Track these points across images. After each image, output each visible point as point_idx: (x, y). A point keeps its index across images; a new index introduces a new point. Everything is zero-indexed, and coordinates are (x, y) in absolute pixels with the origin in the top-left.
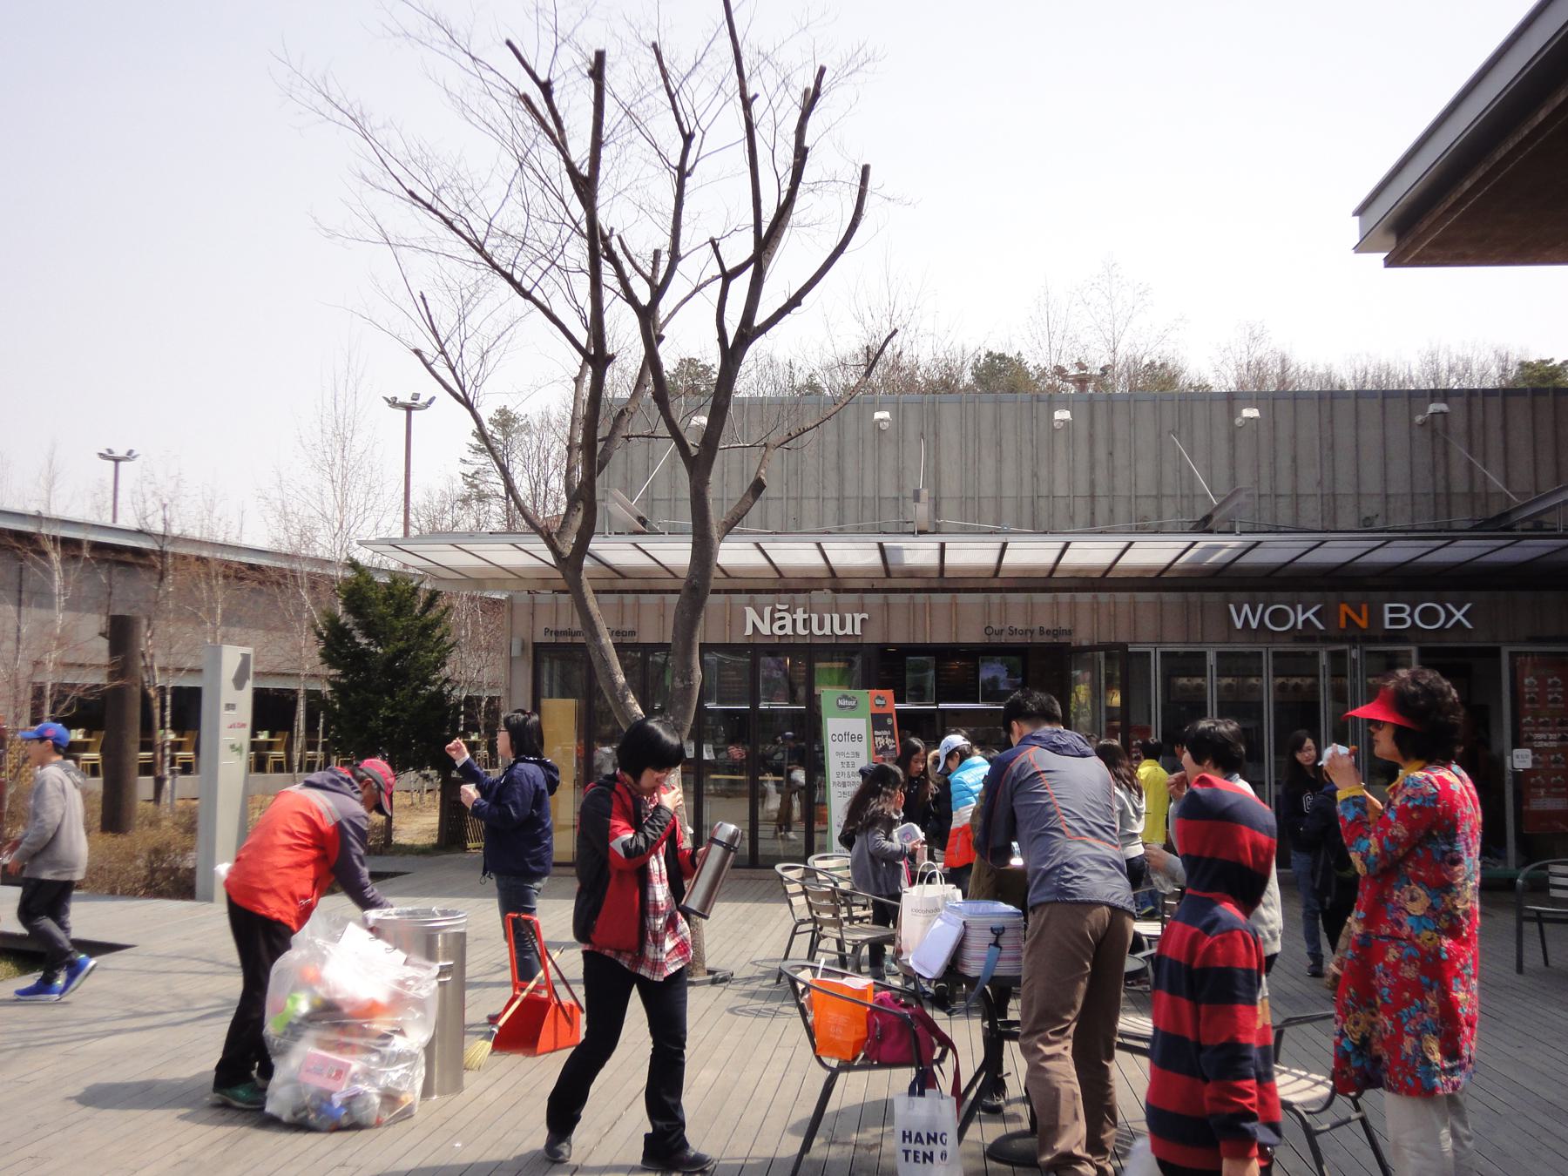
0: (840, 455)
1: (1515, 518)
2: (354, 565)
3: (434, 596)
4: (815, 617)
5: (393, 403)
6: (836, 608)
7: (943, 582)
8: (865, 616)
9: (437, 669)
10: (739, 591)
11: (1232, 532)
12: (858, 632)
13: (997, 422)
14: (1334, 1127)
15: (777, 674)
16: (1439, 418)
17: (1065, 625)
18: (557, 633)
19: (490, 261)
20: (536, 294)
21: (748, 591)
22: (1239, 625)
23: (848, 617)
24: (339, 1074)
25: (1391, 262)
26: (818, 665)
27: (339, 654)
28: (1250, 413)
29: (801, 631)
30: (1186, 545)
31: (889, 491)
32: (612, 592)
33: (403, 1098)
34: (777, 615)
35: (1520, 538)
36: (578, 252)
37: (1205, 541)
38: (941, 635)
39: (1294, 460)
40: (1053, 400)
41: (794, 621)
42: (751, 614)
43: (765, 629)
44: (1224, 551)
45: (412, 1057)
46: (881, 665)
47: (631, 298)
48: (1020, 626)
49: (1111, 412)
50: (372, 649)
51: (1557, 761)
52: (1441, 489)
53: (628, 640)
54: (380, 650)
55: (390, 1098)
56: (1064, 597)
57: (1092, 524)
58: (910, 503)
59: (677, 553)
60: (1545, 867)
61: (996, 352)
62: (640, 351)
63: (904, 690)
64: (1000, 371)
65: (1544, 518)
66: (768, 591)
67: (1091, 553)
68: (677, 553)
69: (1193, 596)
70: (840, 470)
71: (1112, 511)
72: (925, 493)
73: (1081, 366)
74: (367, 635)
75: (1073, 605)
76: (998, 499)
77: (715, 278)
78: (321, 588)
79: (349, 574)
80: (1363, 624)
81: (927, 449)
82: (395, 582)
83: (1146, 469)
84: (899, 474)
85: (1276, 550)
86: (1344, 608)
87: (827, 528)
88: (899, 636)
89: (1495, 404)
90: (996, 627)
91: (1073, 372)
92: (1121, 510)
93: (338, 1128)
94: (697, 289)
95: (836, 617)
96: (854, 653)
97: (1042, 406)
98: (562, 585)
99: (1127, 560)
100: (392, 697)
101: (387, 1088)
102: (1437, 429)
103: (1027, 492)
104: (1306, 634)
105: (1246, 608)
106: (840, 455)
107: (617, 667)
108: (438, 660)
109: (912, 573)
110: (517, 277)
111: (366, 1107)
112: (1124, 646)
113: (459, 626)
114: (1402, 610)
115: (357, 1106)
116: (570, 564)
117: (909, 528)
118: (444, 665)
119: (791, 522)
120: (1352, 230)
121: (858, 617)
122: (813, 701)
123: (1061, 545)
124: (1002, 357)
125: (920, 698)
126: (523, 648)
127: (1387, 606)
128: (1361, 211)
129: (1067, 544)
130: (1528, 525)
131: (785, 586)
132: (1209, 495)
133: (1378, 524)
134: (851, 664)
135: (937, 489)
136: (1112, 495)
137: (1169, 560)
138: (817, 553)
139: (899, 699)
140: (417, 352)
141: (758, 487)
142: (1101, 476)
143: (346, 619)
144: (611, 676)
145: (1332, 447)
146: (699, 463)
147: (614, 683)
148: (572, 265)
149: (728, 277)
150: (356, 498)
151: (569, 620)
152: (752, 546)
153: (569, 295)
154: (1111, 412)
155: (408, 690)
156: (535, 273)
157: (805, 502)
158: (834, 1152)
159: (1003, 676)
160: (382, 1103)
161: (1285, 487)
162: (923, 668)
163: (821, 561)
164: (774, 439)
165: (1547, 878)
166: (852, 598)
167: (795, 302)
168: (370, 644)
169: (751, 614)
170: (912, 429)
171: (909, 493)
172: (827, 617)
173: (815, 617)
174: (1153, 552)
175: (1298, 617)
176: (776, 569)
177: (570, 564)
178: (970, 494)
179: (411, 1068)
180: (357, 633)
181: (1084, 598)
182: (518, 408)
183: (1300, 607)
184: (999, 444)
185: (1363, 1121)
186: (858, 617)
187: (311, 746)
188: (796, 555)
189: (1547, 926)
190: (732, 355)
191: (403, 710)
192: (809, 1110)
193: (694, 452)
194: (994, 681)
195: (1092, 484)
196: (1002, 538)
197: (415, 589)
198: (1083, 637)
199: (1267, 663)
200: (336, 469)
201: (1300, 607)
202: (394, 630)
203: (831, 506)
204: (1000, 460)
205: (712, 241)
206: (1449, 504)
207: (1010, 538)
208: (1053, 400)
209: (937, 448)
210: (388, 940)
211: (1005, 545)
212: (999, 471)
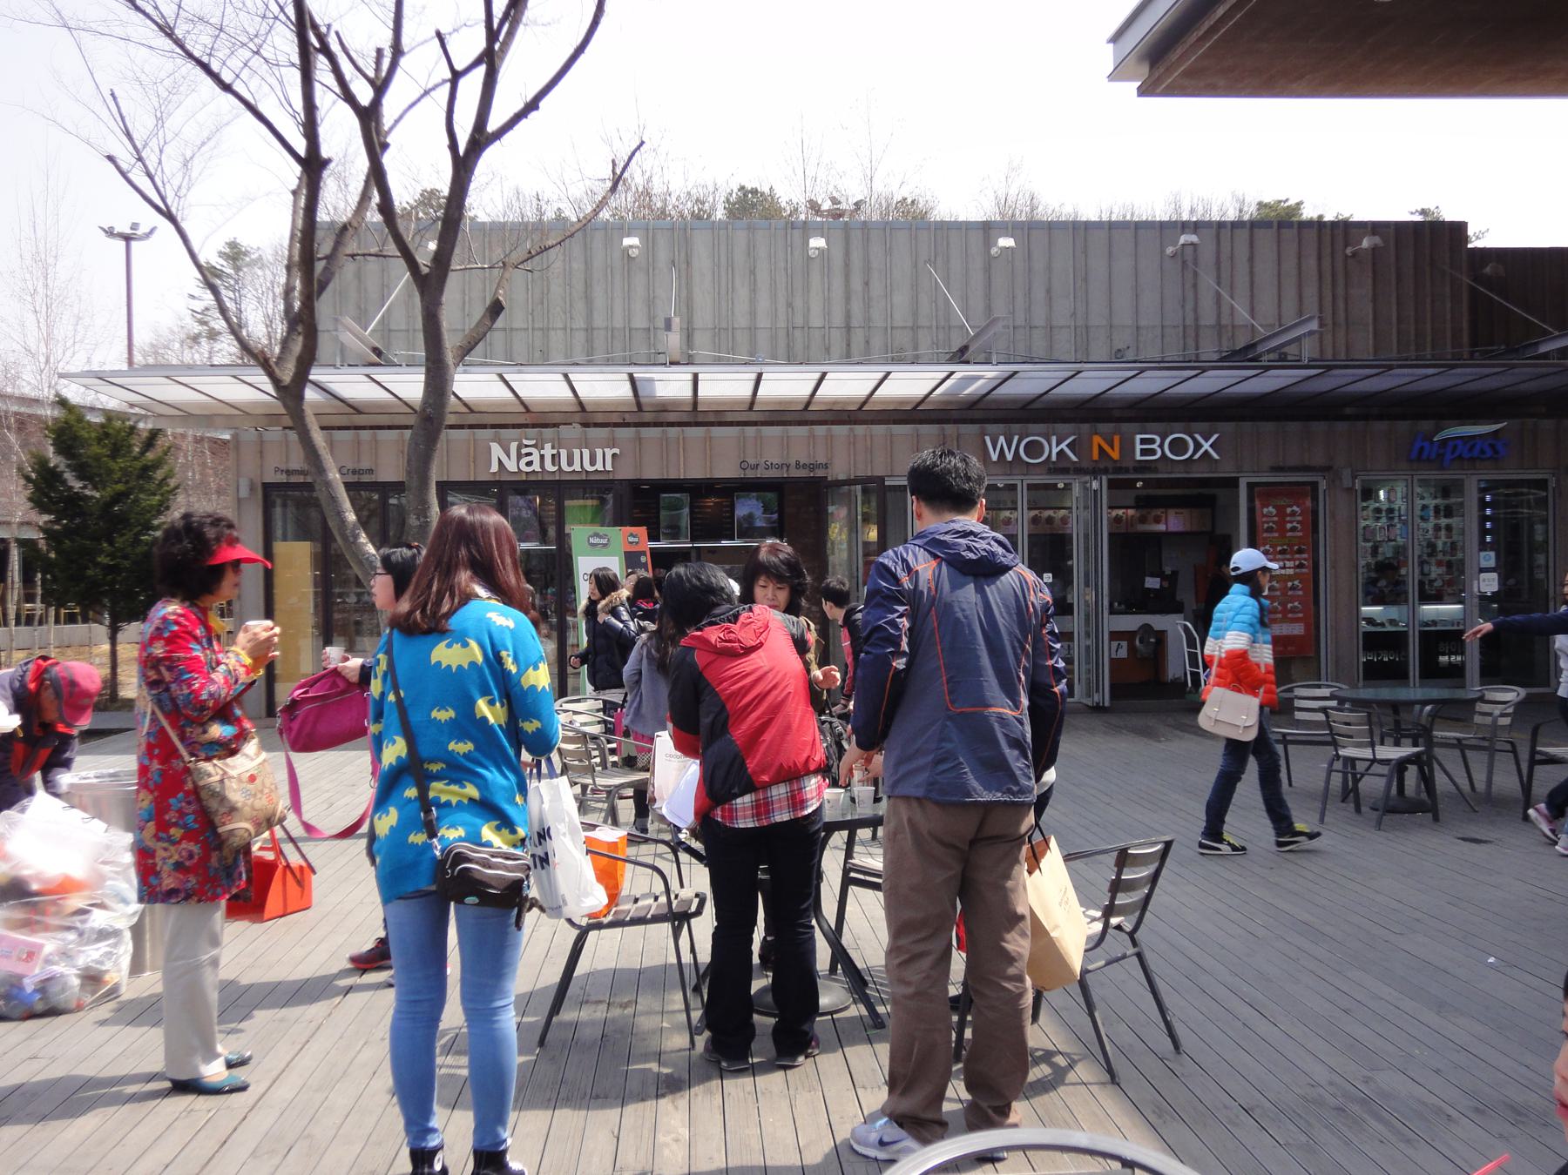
0: (588, 285)
1: (1261, 349)
2: (62, 402)
3: (154, 434)
4: (564, 453)
5: (110, 233)
6: (585, 443)
7: (697, 415)
8: (617, 451)
9: (159, 513)
10: (484, 427)
11: (988, 362)
12: (609, 467)
13: (751, 250)
14: (1108, 964)
15: (526, 514)
16: (1189, 250)
17: (821, 460)
18: (288, 472)
19: (182, 47)
20: (238, 87)
21: (494, 426)
22: (995, 457)
23: (599, 452)
24: (31, 955)
25: (1144, 92)
26: (567, 503)
27: (50, 498)
28: (1006, 242)
29: (549, 467)
30: (944, 375)
31: (640, 322)
32: (347, 428)
33: (107, 977)
34: (524, 451)
35: (1267, 368)
36: (285, 43)
37: (962, 371)
38: (695, 471)
39: (1049, 291)
40: (807, 229)
41: (542, 457)
42: (496, 451)
43: (511, 466)
44: (981, 382)
45: (116, 933)
46: (636, 502)
47: (349, 97)
48: (776, 461)
49: (867, 240)
50: (88, 492)
51: (1293, 588)
52: (1190, 321)
53: (366, 478)
54: (97, 495)
55: (92, 978)
56: (820, 430)
57: (848, 355)
58: (662, 335)
59: (411, 386)
60: (1290, 690)
61: (749, 187)
62: (362, 164)
63: (658, 528)
64: (753, 205)
65: (1286, 349)
66: (515, 426)
67: (847, 384)
68: (411, 386)
69: (950, 429)
70: (588, 299)
71: (867, 342)
72: (676, 321)
73: (834, 201)
74: (80, 478)
75: (830, 438)
76: (752, 330)
77: (444, 81)
78: (31, 429)
79: (57, 413)
80: (1115, 455)
81: (679, 278)
82: (109, 419)
83: (901, 299)
84: (650, 303)
85: (1032, 381)
86: (1097, 440)
87: (576, 360)
88: (652, 472)
89: (1243, 235)
90: (752, 461)
91: (827, 205)
92: (877, 342)
93: (32, 1016)
94: (426, 93)
95: (586, 453)
96: (609, 490)
97: (797, 233)
98: (288, 421)
99: (886, 391)
100: (111, 543)
101: (87, 969)
102: (1187, 260)
103: (782, 324)
104: (1060, 467)
105: (1002, 439)
106: (588, 285)
107: (347, 505)
108: (161, 503)
109: (664, 407)
110: (215, 67)
111: (63, 990)
112: (882, 479)
113: (185, 467)
114: (1152, 441)
115: (54, 989)
116: (291, 393)
117: (661, 358)
118: (168, 508)
119: (538, 354)
120: (1107, 57)
121: (609, 452)
122: (563, 539)
123: (817, 376)
124: (754, 192)
125: (675, 534)
126: (252, 489)
127: (1138, 437)
128: (1116, 38)
129: (824, 374)
130: (1272, 356)
131: (533, 420)
132: (965, 323)
133: (1130, 355)
134: (603, 501)
135: (690, 321)
136: (868, 326)
137: (925, 392)
138: (565, 384)
139: (653, 537)
140: (110, 158)
141: (496, 309)
142: (857, 307)
143: (54, 460)
144: (340, 514)
145: (1086, 280)
146: (430, 283)
147: (343, 521)
148: (282, 59)
149: (456, 76)
150: (63, 329)
151: (297, 461)
152: (496, 378)
153: (279, 94)
154: (867, 240)
155: (129, 536)
156: (235, 63)
157: (552, 333)
158: (585, 1014)
159: (758, 512)
160: (82, 986)
161: (1039, 319)
162: (676, 506)
163: (570, 394)
164: (517, 256)
165: (1291, 700)
166: (603, 432)
167: (532, 105)
168: (85, 487)
169: (496, 451)
170: (663, 256)
171: (661, 324)
172: (577, 452)
173: (564, 453)
174: (911, 383)
175: (1052, 449)
176: (522, 403)
177: (291, 393)
178: (724, 325)
179: (115, 945)
180: (68, 476)
181: (840, 430)
182: (245, 242)
183: (1054, 439)
184: (753, 272)
185: (1139, 955)
186: (609, 452)
187: (30, 598)
188: (542, 387)
189: (1469, 753)
190: (463, 166)
191: (125, 557)
192: (554, 975)
193: (425, 270)
194: (750, 517)
195: (848, 316)
196: (758, 369)
197: (133, 428)
198: (839, 472)
199: (1022, 497)
200: (38, 299)
201: (1054, 439)
202: (110, 472)
203: (580, 337)
204: (754, 290)
205: (439, 35)
206: (1197, 336)
207: (765, 369)
208: (807, 229)
209: (689, 277)
210: (84, 809)
211: (760, 376)
212: (753, 301)
